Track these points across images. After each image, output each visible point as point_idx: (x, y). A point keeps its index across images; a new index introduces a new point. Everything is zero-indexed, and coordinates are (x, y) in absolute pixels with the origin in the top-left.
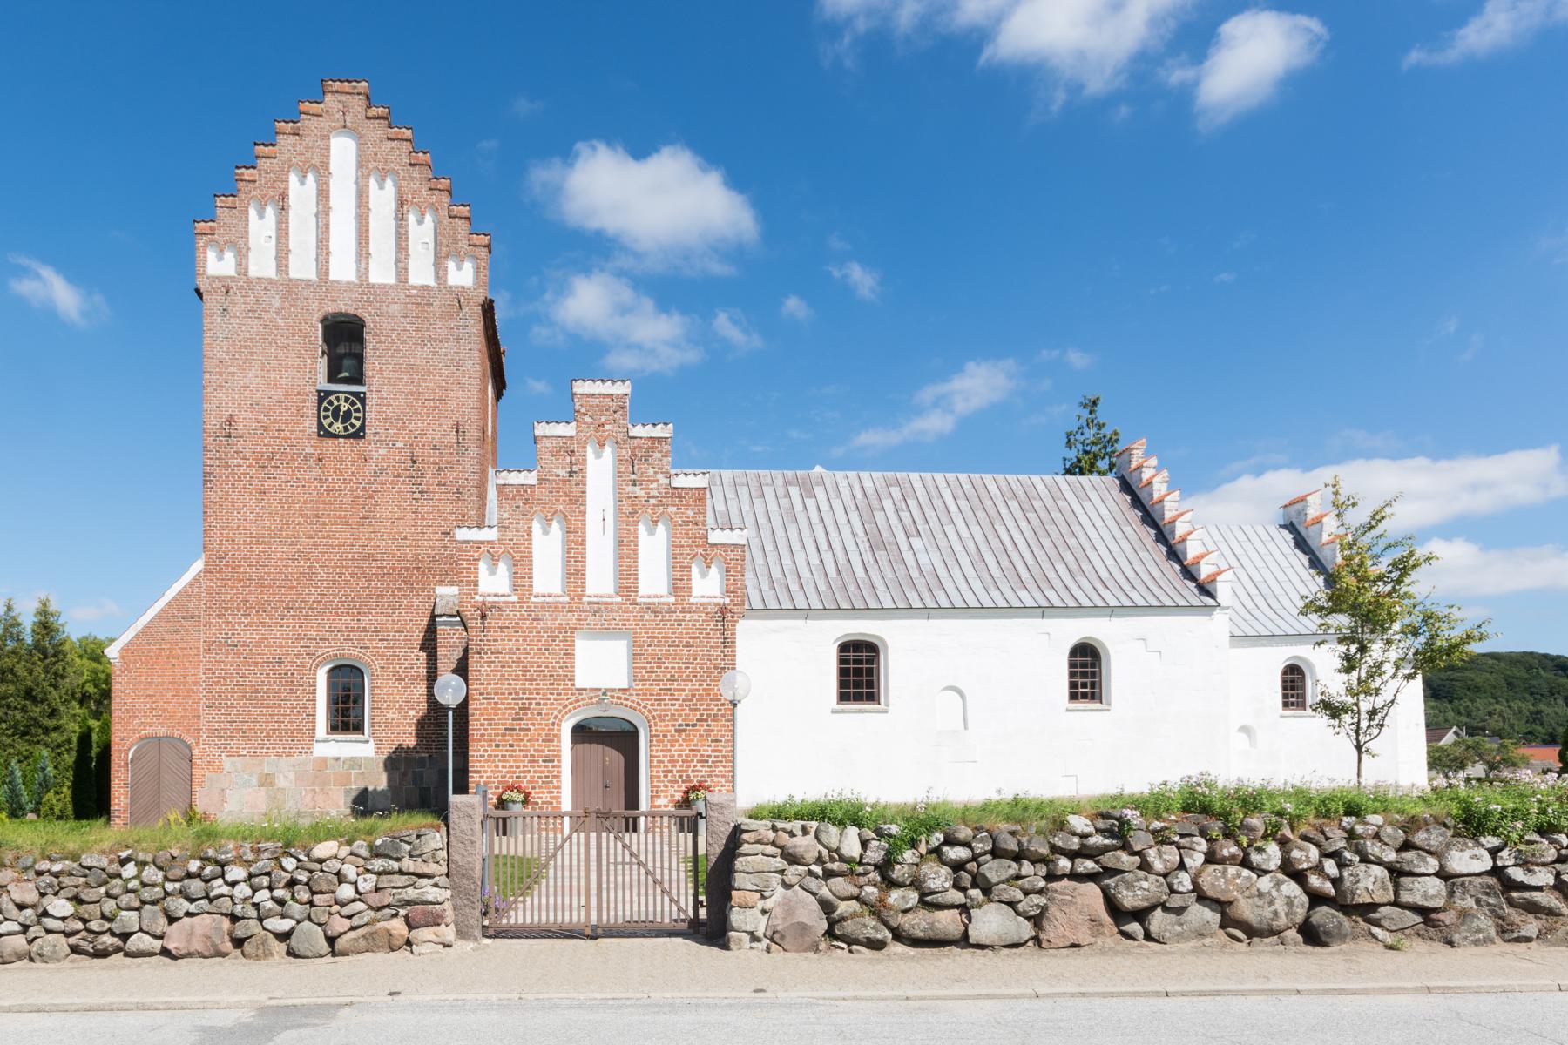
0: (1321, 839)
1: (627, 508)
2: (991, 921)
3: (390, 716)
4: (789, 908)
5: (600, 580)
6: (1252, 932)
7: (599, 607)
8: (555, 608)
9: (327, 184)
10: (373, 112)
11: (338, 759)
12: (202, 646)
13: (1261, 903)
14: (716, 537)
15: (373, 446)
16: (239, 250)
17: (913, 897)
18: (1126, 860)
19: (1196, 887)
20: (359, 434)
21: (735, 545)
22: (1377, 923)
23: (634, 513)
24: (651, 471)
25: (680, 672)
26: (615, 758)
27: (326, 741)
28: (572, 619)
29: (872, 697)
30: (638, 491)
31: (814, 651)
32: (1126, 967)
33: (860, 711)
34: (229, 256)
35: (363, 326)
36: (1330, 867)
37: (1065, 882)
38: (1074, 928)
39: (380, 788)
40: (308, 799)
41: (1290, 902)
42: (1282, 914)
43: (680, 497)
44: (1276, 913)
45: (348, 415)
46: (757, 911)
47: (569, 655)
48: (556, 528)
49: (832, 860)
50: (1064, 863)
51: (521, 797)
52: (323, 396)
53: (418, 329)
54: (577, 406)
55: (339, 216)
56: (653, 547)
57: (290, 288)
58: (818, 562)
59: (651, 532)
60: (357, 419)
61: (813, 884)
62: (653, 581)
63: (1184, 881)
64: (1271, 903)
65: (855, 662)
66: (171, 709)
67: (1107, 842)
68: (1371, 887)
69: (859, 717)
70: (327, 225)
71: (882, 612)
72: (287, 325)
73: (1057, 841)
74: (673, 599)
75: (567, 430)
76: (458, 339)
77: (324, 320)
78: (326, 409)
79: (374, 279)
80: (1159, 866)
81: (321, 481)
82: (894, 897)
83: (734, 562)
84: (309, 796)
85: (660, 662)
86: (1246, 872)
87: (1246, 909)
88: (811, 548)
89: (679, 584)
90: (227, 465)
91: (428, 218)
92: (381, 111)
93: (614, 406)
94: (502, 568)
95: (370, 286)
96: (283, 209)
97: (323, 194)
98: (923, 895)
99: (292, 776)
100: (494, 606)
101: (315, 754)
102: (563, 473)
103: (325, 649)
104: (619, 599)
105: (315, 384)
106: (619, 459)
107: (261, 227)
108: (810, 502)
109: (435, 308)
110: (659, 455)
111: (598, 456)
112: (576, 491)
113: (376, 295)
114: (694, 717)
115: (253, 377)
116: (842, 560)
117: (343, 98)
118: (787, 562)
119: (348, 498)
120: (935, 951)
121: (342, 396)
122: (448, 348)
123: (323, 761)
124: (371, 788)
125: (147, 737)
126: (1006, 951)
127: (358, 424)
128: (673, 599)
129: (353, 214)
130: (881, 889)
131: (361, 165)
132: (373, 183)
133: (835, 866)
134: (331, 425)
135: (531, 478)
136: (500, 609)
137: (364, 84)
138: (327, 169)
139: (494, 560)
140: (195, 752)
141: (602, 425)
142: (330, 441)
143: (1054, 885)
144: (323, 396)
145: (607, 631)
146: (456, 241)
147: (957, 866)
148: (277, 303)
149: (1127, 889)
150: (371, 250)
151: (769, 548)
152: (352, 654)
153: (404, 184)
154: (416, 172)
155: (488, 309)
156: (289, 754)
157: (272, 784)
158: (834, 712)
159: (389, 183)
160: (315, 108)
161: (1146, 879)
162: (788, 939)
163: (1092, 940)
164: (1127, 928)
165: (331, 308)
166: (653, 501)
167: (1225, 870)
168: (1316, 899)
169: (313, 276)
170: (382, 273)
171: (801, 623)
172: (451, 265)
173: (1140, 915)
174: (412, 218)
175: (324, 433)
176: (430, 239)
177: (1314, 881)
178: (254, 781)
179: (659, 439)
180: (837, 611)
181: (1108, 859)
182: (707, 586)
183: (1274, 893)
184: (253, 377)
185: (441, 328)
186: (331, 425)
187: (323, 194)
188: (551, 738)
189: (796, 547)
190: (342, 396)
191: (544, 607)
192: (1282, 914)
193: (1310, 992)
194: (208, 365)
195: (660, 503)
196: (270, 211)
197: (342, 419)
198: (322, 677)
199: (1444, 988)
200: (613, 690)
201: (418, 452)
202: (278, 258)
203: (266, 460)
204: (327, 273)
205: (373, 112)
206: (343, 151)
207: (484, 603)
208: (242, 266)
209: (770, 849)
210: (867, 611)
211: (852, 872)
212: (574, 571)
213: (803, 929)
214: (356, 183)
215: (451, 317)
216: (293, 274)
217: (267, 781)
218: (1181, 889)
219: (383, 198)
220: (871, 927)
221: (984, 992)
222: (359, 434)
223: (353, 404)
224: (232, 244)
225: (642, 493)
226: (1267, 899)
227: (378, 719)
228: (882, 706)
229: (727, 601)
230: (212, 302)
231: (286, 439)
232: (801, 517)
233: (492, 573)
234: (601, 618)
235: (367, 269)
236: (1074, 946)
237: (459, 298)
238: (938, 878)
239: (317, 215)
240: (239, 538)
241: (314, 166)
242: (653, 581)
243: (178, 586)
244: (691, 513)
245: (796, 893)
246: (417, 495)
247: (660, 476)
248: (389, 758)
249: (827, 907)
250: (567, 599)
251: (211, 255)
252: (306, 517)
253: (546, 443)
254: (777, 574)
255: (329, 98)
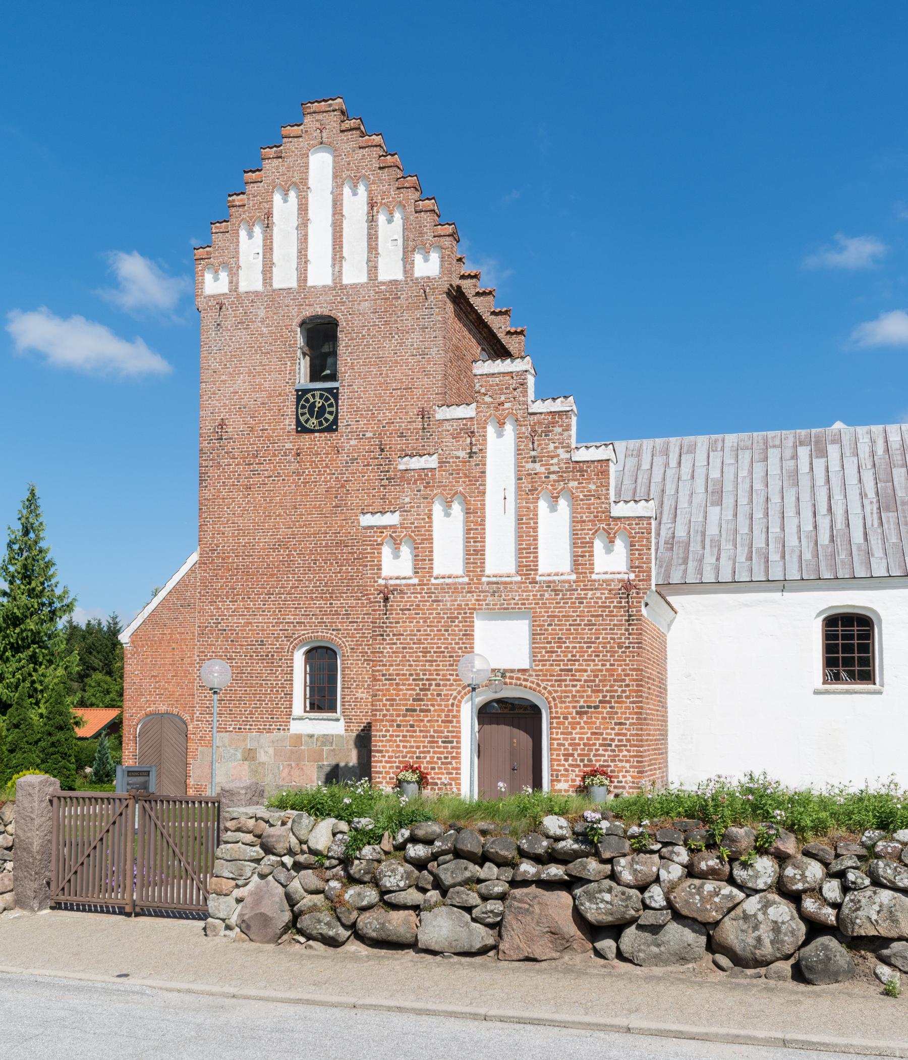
0: (830, 857)
1: (527, 486)
2: (441, 926)
3: (359, 695)
4: (258, 896)
5: (500, 560)
6: (740, 961)
7: (499, 586)
8: (455, 589)
9: (306, 198)
10: (347, 124)
11: (311, 736)
12: (197, 630)
13: (745, 927)
14: (618, 510)
15: (346, 439)
16: (231, 269)
17: (371, 895)
18: (593, 865)
19: (670, 905)
20: (332, 427)
21: (640, 518)
22: (886, 961)
23: (533, 490)
24: (552, 446)
25: (582, 651)
26: (523, 739)
27: (301, 719)
28: (472, 599)
29: (867, 676)
30: (538, 468)
31: (797, 626)
32: (593, 988)
33: (848, 692)
34: (224, 276)
35: (337, 325)
36: (832, 890)
37: (533, 889)
38: (531, 940)
39: (351, 764)
40: (285, 773)
41: (776, 928)
42: (767, 942)
43: (581, 471)
44: (759, 939)
45: (322, 409)
46: (231, 900)
47: (468, 635)
48: (457, 508)
49: (303, 852)
50: (528, 868)
51: (415, 777)
52: (301, 394)
53: (386, 323)
54: (477, 387)
55: (326, 227)
56: (555, 524)
57: (272, 297)
58: (810, 528)
59: (553, 509)
60: (331, 413)
61: (282, 875)
62: (554, 557)
63: (656, 896)
64: (756, 928)
65: (845, 637)
66: (170, 688)
67: (576, 846)
68: (874, 917)
69: (851, 701)
70: (306, 235)
71: (871, 581)
72: (271, 333)
73: (524, 844)
74: (574, 577)
75: (466, 411)
76: (424, 328)
77: (302, 324)
78: (303, 407)
79: (347, 280)
80: (627, 876)
81: (299, 474)
82: (351, 893)
83: (637, 534)
84: (287, 770)
85: (560, 641)
86: (727, 890)
87: (731, 932)
88: (806, 513)
89: (581, 557)
90: (219, 465)
91: (397, 216)
92: (353, 123)
93: (513, 383)
94: (620, 546)
95: (343, 287)
96: (268, 227)
97: (303, 208)
98: (383, 892)
99: (271, 751)
100: (394, 589)
101: (292, 732)
102: (462, 454)
103: (301, 632)
104: (519, 578)
105: (293, 384)
106: (519, 437)
107: (249, 245)
108: (819, 464)
109: (402, 301)
110: (559, 430)
111: (500, 435)
112: (476, 472)
113: (348, 295)
114: (596, 699)
115: (241, 383)
116: (840, 524)
117: (320, 117)
118: (775, 529)
119: (322, 489)
120: (383, 952)
121: (318, 393)
122: (414, 338)
123: (299, 737)
124: (342, 764)
125: (151, 714)
126: (456, 959)
127: (331, 418)
128: (574, 577)
129: (330, 222)
130: (344, 885)
131: (335, 176)
132: (347, 190)
133: (301, 858)
134: (307, 421)
135: (431, 462)
136: (402, 592)
137: (339, 100)
138: (306, 184)
139: (397, 545)
140: (190, 727)
141: (502, 404)
142: (307, 436)
143: (518, 892)
144: (301, 394)
145: (506, 612)
146: (421, 234)
147: (420, 864)
148: (262, 313)
149: (590, 901)
150: (345, 254)
151: (758, 515)
152: (325, 636)
153: (374, 187)
154: (384, 175)
155: (458, 297)
156: (269, 731)
157: (254, 759)
158: (817, 692)
159: (362, 189)
160: (296, 130)
161: (610, 890)
162: (253, 929)
163: (556, 955)
164: (598, 945)
165: (308, 312)
166: (553, 477)
167: (702, 886)
168: (815, 928)
169: (294, 284)
170: (354, 274)
171: (777, 595)
172: (418, 258)
173: (615, 930)
174: (382, 218)
175: (302, 429)
176: (399, 236)
177: (809, 904)
178: (239, 756)
179: (560, 413)
180: (817, 582)
181: (575, 867)
182: (611, 561)
183: (760, 917)
184: (241, 383)
185: (408, 319)
186: (307, 421)
187: (303, 208)
188: (451, 719)
189: (790, 512)
190: (318, 393)
191: (444, 588)
192: (767, 942)
193: (642, 1032)
194: (204, 377)
195: (561, 479)
196: (258, 230)
197: (317, 413)
198: (299, 658)
199: (804, 1042)
200: (512, 671)
201: (386, 440)
202: (264, 272)
203: (252, 458)
204: (305, 280)
205: (347, 124)
206: (321, 166)
207: (386, 586)
208: (234, 284)
209: (249, 838)
210: (853, 581)
211: (322, 865)
212: (475, 552)
213: (265, 920)
214: (332, 193)
215: (418, 308)
216: (277, 285)
217: (250, 755)
218: (653, 905)
219: (356, 203)
220: (325, 924)
221: (305, 996)
222: (332, 427)
223: (327, 399)
224: (225, 265)
225: (543, 469)
226: (753, 922)
227: (348, 698)
228: (877, 687)
229: (632, 576)
230: (209, 319)
231: (269, 437)
232: (805, 482)
233: (609, 551)
234: (501, 600)
235: (340, 272)
236: (528, 959)
237: (424, 287)
238: (395, 875)
239: (297, 229)
240: (229, 531)
241: (295, 184)
242: (554, 557)
243: (177, 577)
244: (592, 487)
245: (268, 884)
246: (385, 482)
247: (561, 451)
248: (358, 736)
249: (291, 901)
250: (466, 580)
251: (208, 277)
252: (285, 508)
253: (447, 426)
254: (759, 543)
255: (308, 119)
